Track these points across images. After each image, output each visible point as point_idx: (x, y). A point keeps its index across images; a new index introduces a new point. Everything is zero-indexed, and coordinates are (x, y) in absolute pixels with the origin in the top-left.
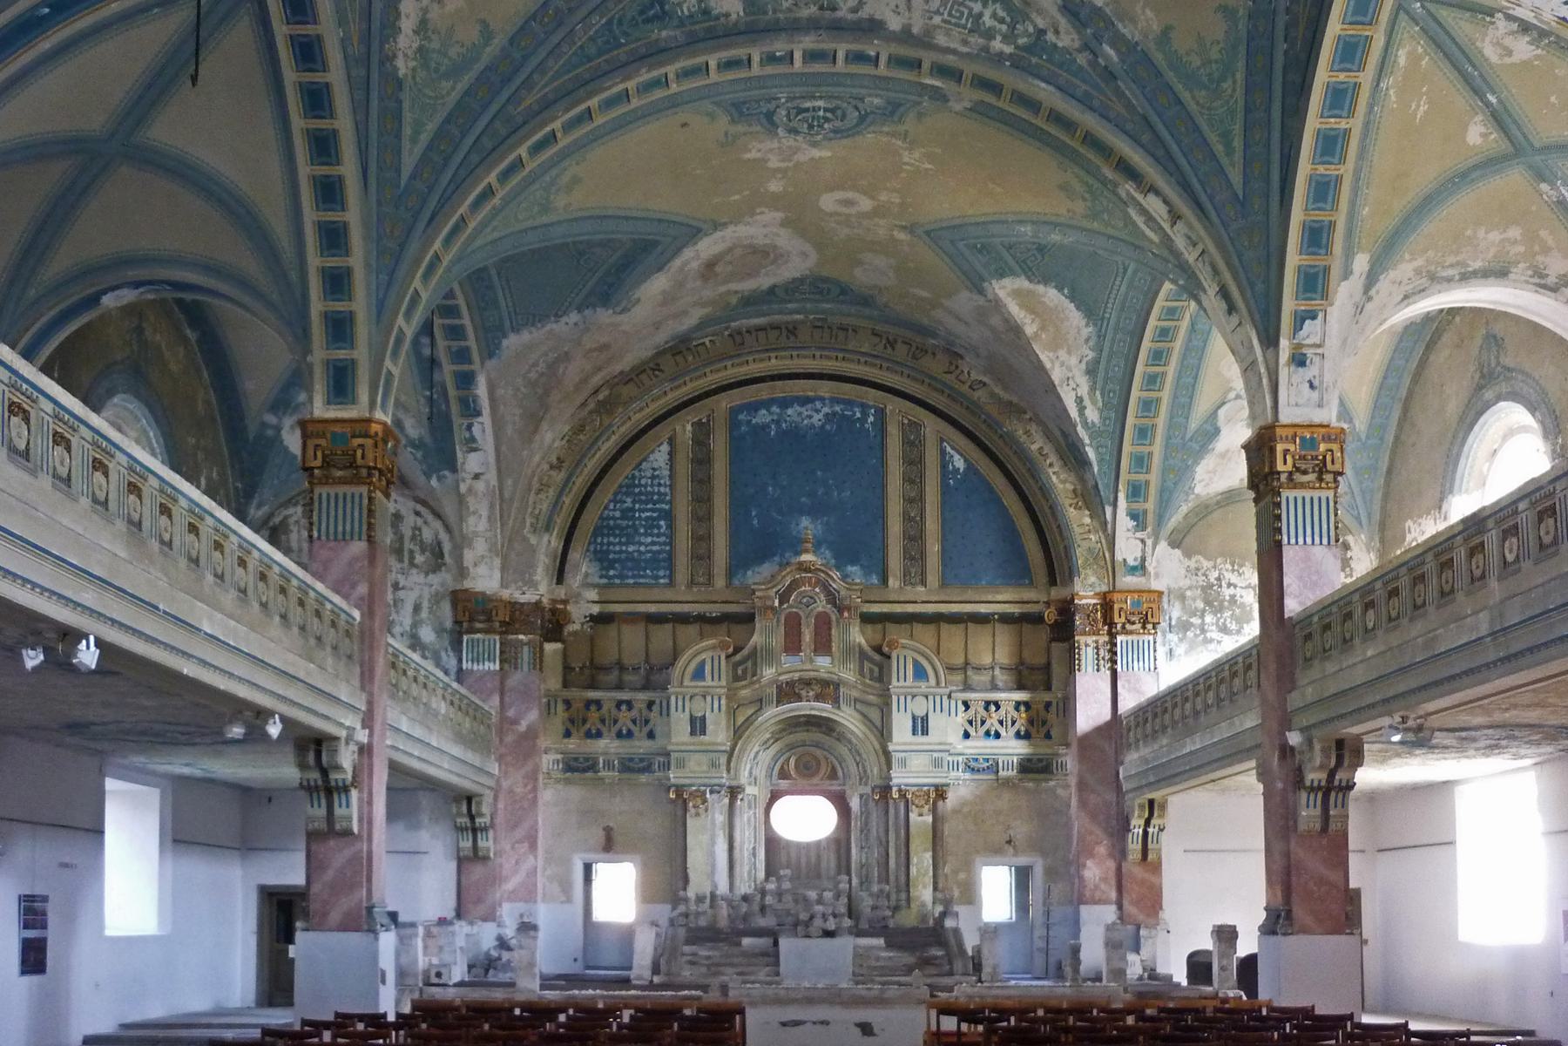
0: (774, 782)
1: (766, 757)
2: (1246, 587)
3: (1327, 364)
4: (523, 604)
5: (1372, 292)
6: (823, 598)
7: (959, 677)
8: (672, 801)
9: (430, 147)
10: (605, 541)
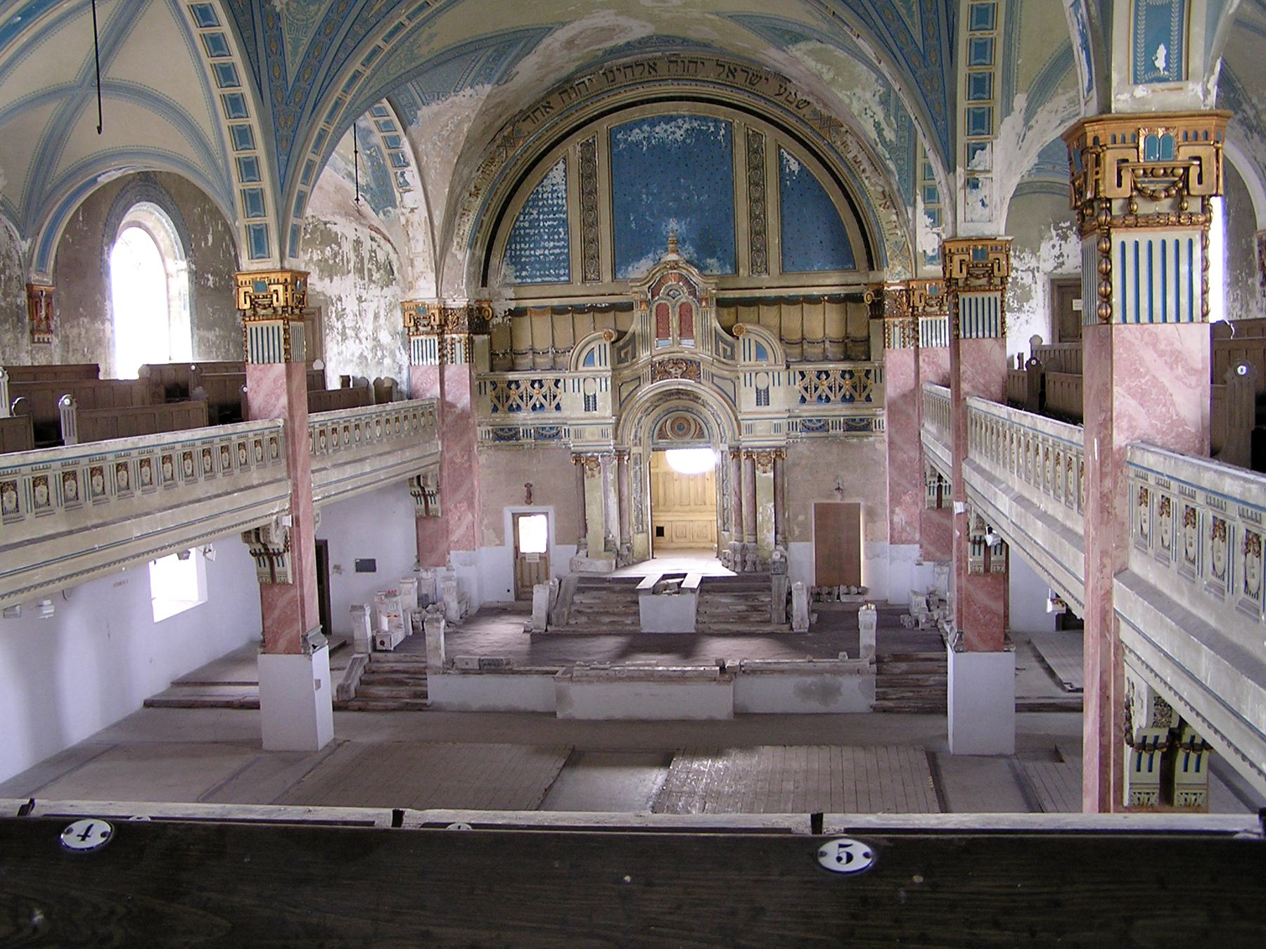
0: (655, 441)
1: (647, 422)
3: (996, 185)
5: (1032, 122)
7: (797, 350)
9: (307, 55)
10: (518, 247)
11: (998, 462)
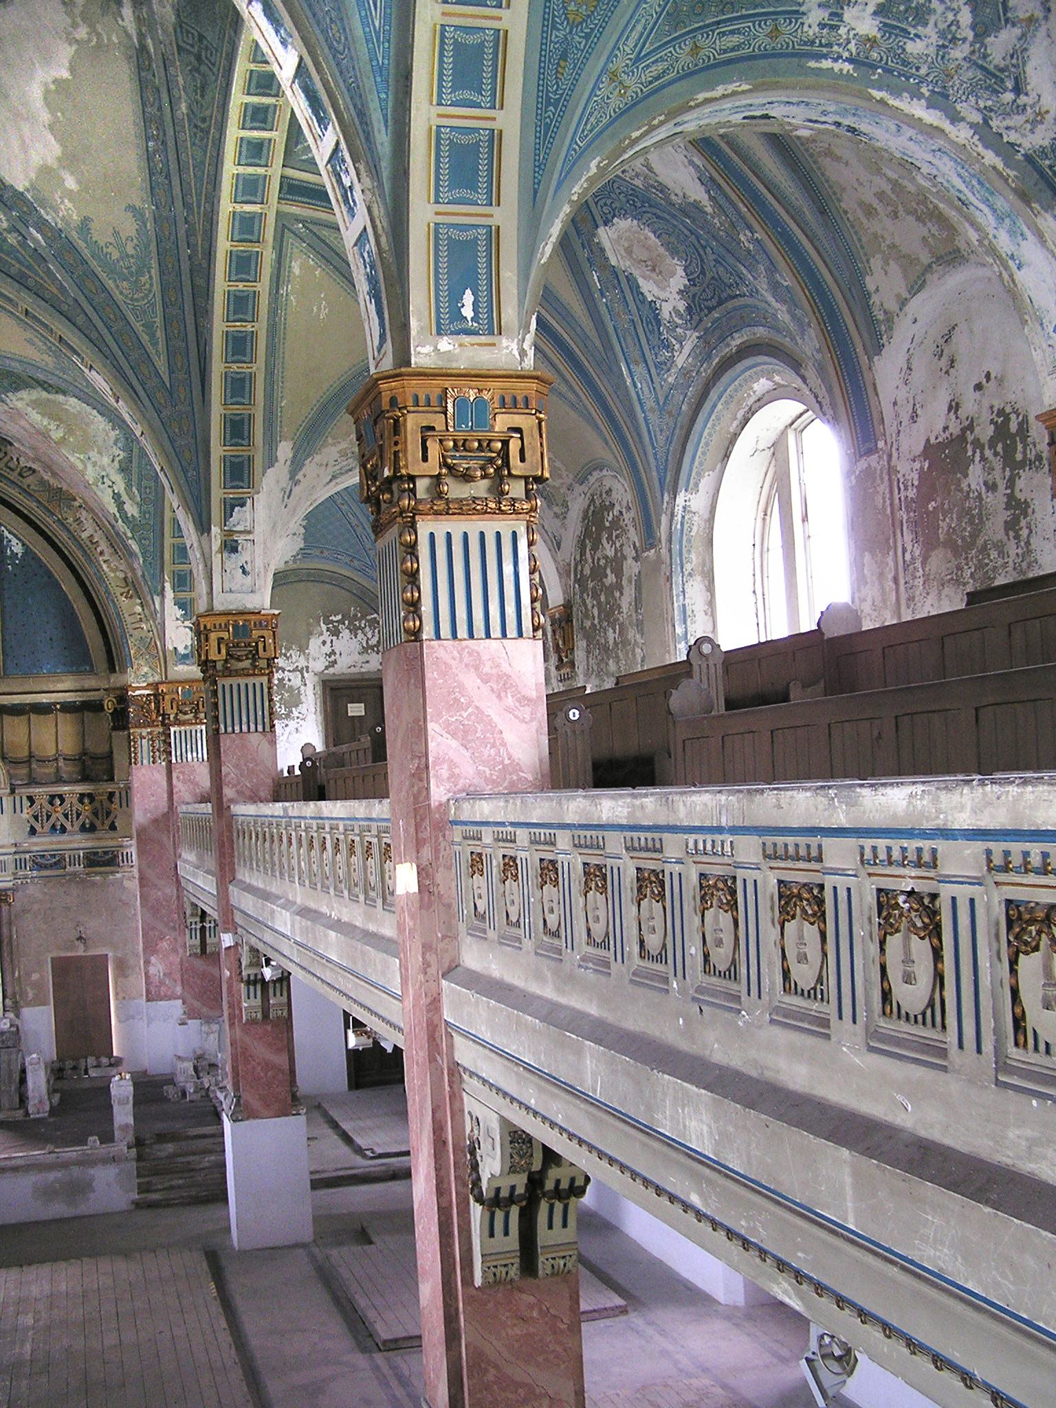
2: (294, 671)
3: (259, 550)
5: (299, 476)
7: (24, 771)
11: (273, 875)
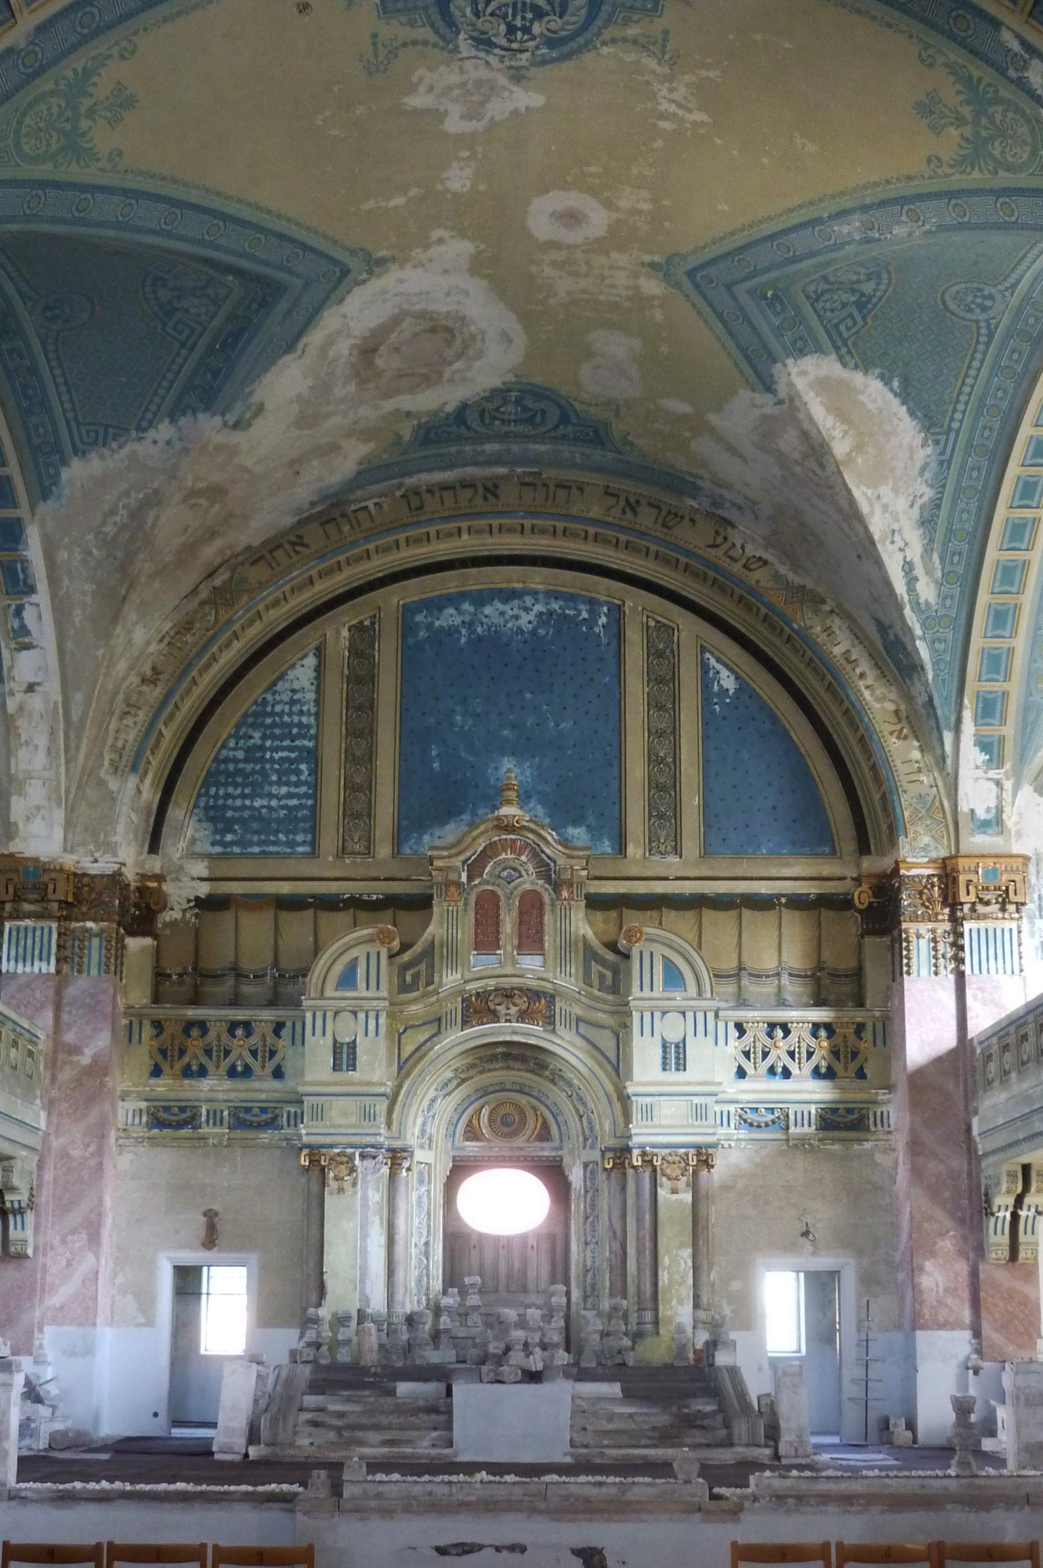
1: (447, 1107)
4: (95, 876)
6: (531, 870)
7: (730, 988)
8: (306, 1170)
10: (221, 792)
